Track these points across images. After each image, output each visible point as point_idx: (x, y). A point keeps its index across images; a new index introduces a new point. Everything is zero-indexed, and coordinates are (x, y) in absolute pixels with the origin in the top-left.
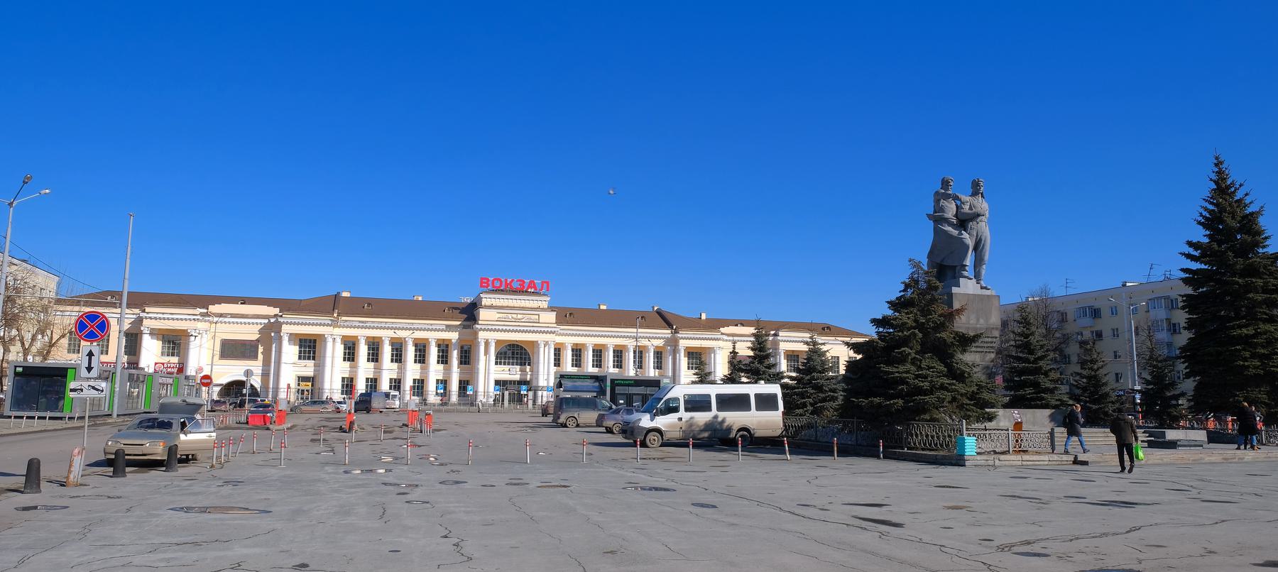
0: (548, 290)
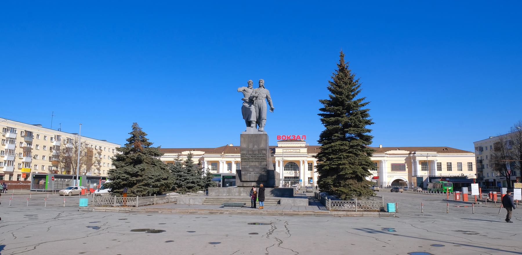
0: (305, 139)
